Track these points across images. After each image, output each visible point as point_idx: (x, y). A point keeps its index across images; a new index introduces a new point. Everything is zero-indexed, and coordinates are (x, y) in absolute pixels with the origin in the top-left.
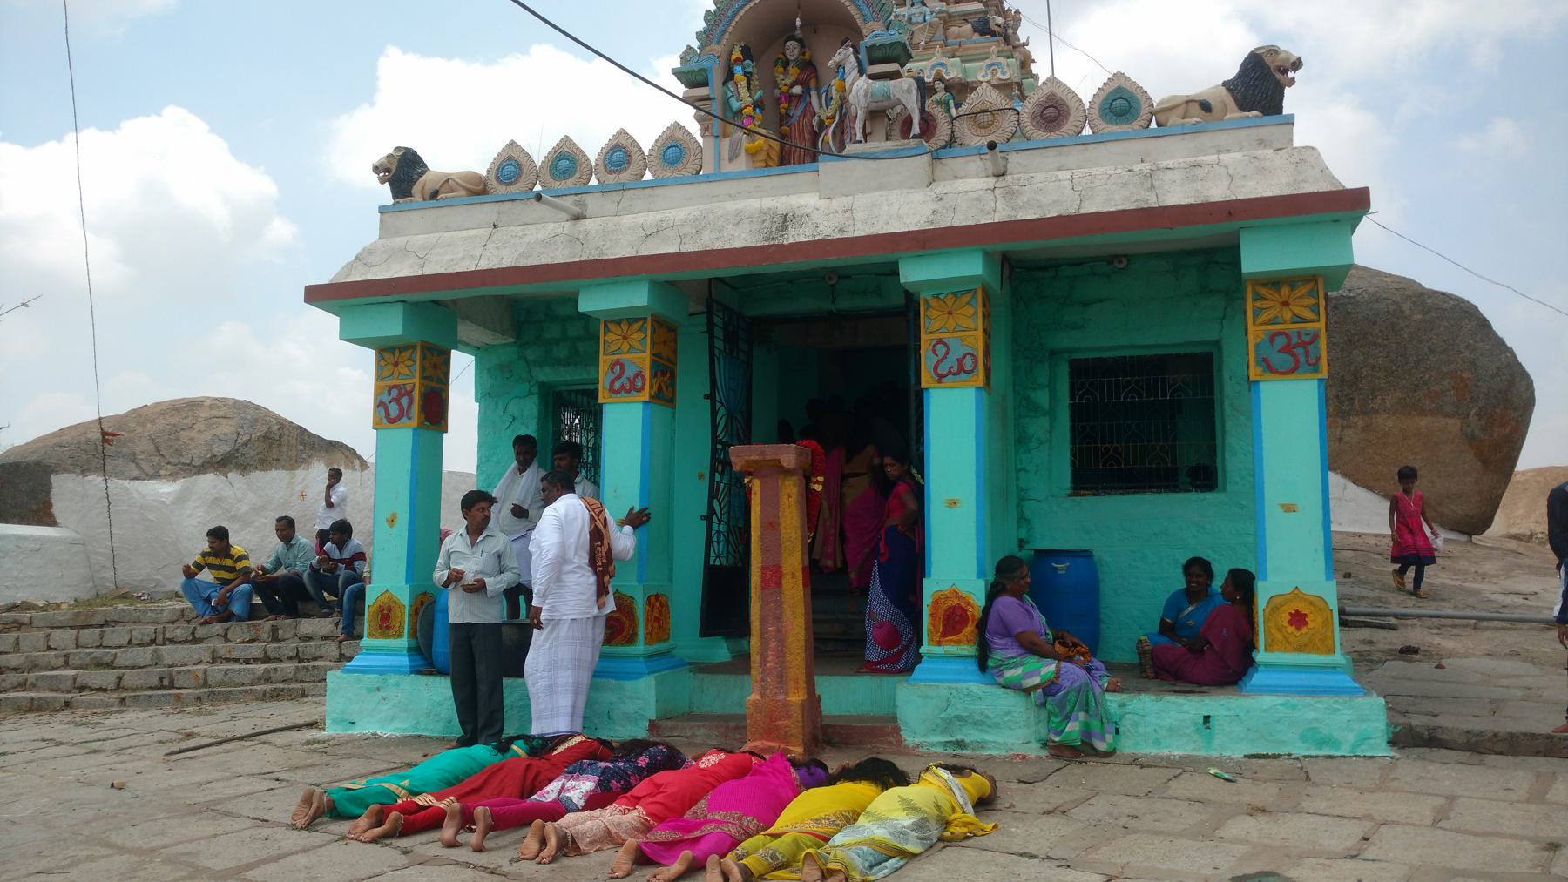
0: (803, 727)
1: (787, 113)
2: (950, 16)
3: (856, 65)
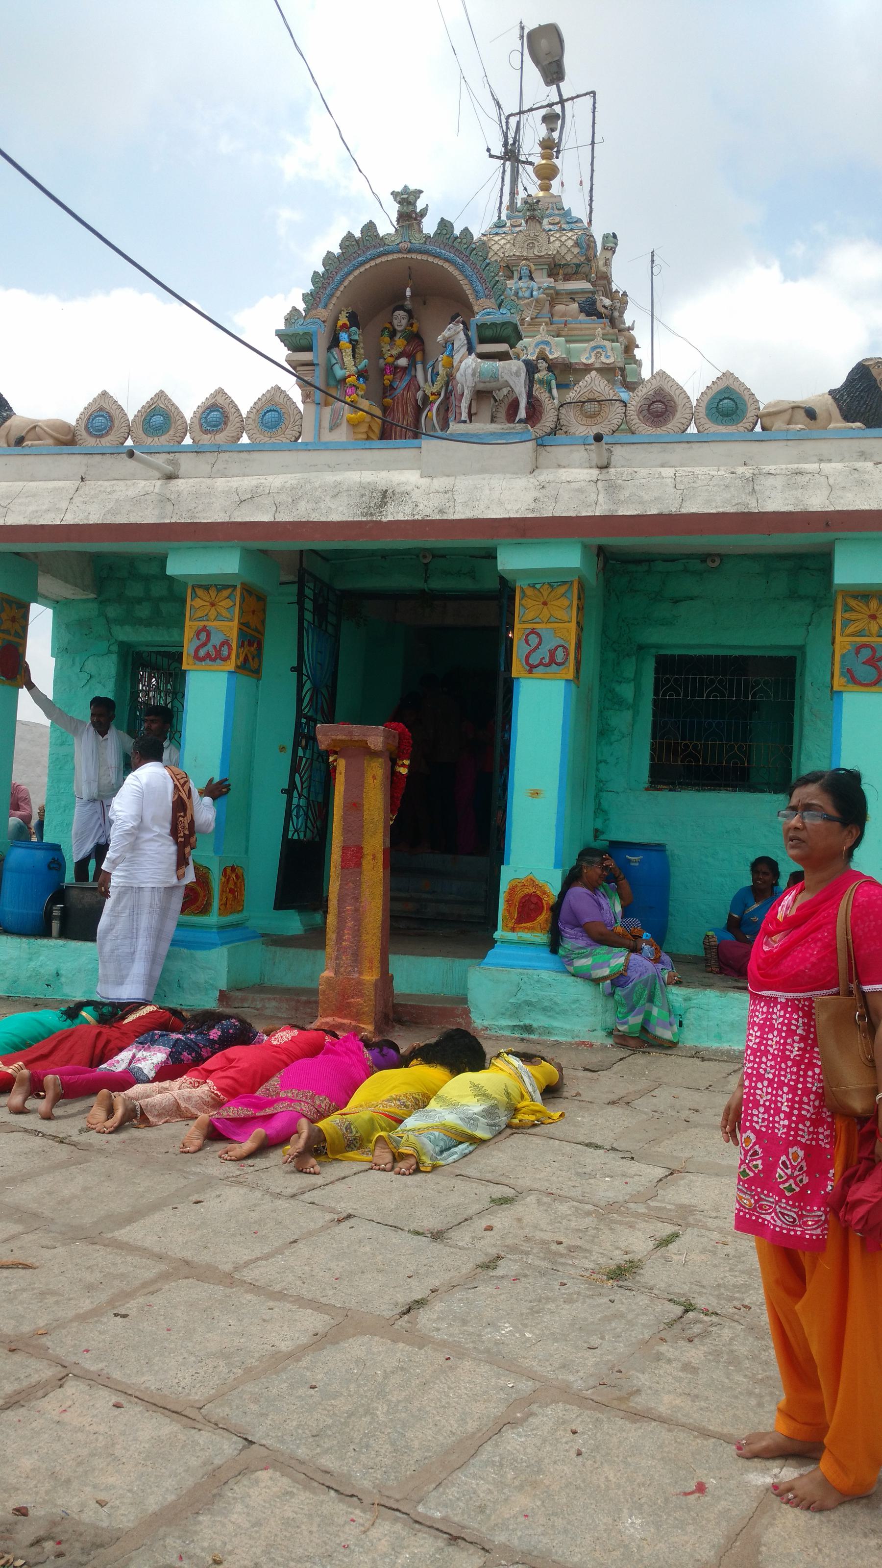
0: (375, 1006)
1: (391, 385)
2: (558, 293)
3: (466, 342)
